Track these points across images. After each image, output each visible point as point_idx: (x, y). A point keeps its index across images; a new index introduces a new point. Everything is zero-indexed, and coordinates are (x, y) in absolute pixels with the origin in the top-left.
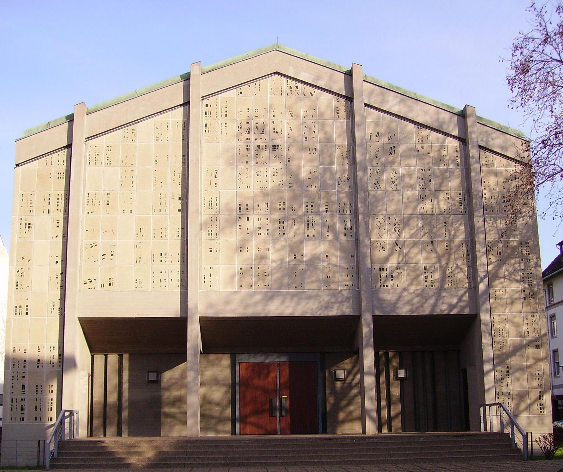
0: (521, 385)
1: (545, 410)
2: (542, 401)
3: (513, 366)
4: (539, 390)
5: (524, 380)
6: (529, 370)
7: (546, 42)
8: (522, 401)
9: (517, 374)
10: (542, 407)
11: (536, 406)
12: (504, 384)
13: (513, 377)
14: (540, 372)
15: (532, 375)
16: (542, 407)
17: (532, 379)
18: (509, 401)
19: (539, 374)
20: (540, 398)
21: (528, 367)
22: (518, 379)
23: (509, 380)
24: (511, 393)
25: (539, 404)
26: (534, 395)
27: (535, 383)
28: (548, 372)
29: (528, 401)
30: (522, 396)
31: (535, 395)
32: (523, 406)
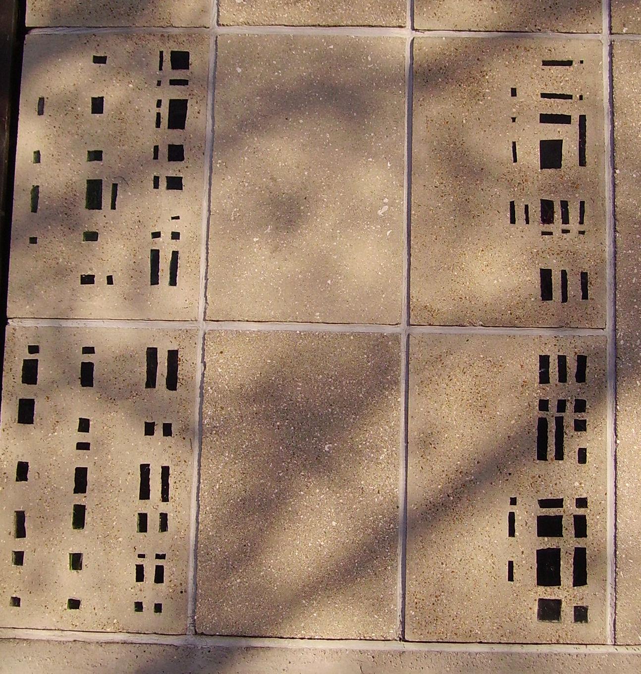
0: (321, 275)
1: (596, 595)
2: (566, 480)
3: (245, 51)
4: (545, 341)
5: (357, 216)
6: (435, 109)
7: (70, 301)
8: (319, 463)
9: (283, 155)
10: (567, 543)
11: (488, 550)
12: (116, 253)
13: (227, 187)
14: (567, 135)
15: (463, 167)
16: (567, 543)
17: (466, 213)
18: (156, 452)
19: (551, 153)
20: (549, 436)
21: (427, 76)
22: (285, 213)
23: (179, 216)
24: (191, 366)
25: (527, 515)
26: (465, 407)
27: (498, 266)
28: (463, 383)
29: (389, 477)
30: (306, 417)
31: (481, 405)
32: (314, 531)
